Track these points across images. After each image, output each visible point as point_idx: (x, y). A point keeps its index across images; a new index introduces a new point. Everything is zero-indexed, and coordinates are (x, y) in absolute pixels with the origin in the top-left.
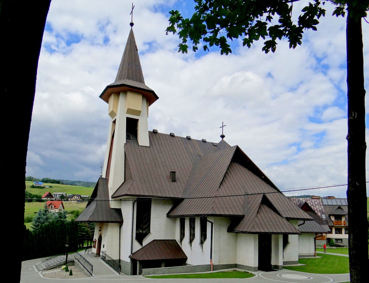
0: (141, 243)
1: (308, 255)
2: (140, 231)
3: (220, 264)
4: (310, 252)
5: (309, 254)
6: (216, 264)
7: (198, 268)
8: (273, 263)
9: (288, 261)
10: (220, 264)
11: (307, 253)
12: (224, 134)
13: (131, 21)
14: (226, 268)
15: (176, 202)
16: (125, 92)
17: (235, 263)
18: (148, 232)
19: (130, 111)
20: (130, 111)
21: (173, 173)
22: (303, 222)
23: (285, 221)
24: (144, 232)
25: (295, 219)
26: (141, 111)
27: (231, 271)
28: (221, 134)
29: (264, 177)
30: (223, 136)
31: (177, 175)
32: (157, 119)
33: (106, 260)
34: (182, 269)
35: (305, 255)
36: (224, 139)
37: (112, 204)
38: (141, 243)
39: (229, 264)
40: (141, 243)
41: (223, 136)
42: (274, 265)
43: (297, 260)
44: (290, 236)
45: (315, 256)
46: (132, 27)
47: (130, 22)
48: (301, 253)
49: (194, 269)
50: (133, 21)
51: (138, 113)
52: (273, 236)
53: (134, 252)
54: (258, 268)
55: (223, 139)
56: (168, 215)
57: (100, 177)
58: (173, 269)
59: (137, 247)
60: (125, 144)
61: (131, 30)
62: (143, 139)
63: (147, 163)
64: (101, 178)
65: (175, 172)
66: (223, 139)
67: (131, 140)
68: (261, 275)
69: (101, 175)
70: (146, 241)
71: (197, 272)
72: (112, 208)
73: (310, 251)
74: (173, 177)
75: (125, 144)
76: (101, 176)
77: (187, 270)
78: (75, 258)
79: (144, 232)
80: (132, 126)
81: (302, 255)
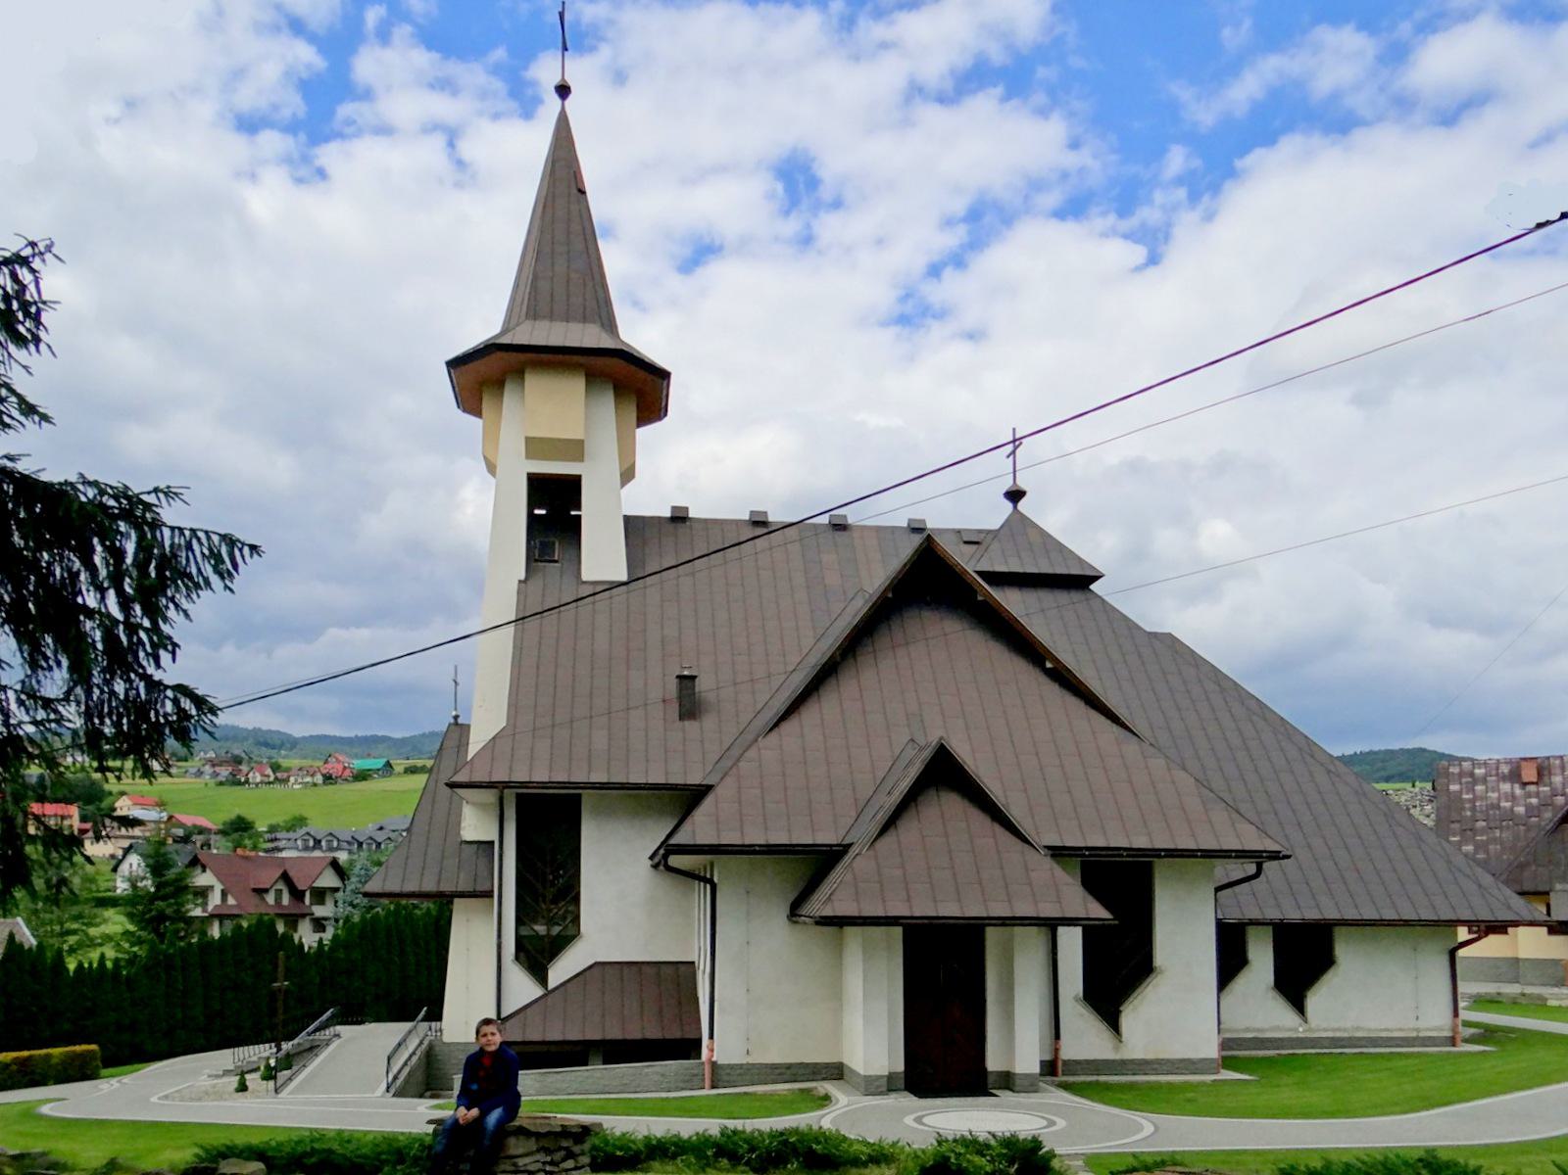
0: (541, 976)
1: (1290, 1039)
2: (536, 928)
3: (751, 1060)
4: (1421, 1024)
5: (1414, 1034)
6: (733, 1062)
7: (647, 1074)
8: (994, 1063)
9: (1150, 1056)
10: (751, 1062)
11: (1401, 1030)
12: (1022, 484)
13: (560, 77)
14: (786, 1077)
15: (688, 798)
16: (519, 373)
17: (835, 1061)
18: (571, 932)
19: (535, 447)
20: (535, 447)
21: (686, 681)
22: (1252, 869)
23: (1048, 863)
24: (556, 930)
25: (1230, 857)
26: (582, 438)
27: (785, 1092)
28: (1007, 484)
29: (1051, 662)
30: (1015, 495)
31: (703, 685)
32: (683, 466)
33: (444, 1043)
34: (587, 1078)
35: (1384, 1034)
36: (1022, 505)
37: (470, 826)
38: (539, 972)
39: (799, 1061)
40: (541, 976)
41: (1015, 495)
42: (1002, 1072)
43: (1212, 1051)
44: (1061, 930)
45: (1454, 1045)
46: (567, 102)
47: (556, 80)
48: (1358, 1029)
49: (634, 1080)
50: (566, 78)
51: (575, 449)
52: (992, 935)
53: (509, 1013)
54: (885, 1079)
55: (1015, 507)
56: (663, 859)
57: (452, 721)
58: (555, 1075)
59: (522, 989)
60: (520, 581)
61: (560, 113)
62: (602, 554)
63: (592, 651)
64: (456, 724)
65: (693, 678)
66: (1015, 507)
67: (556, 564)
68: (1141, 1125)
69: (454, 713)
70: (561, 970)
71: (609, 1093)
72: (468, 839)
73: (1417, 1018)
74: (688, 701)
75: (520, 581)
76: (456, 717)
77: (607, 1083)
78: (429, 1033)
79: (556, 930)
80: (554, 508)
81: (1365, 1034)
